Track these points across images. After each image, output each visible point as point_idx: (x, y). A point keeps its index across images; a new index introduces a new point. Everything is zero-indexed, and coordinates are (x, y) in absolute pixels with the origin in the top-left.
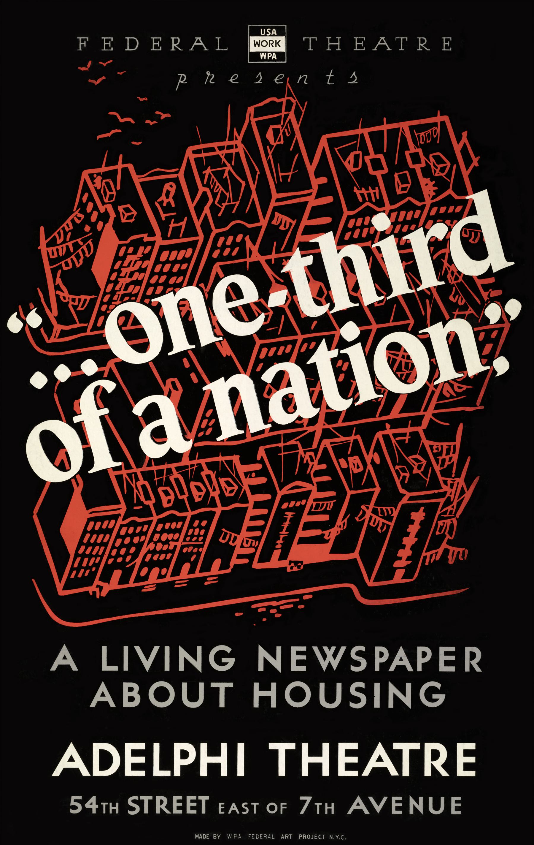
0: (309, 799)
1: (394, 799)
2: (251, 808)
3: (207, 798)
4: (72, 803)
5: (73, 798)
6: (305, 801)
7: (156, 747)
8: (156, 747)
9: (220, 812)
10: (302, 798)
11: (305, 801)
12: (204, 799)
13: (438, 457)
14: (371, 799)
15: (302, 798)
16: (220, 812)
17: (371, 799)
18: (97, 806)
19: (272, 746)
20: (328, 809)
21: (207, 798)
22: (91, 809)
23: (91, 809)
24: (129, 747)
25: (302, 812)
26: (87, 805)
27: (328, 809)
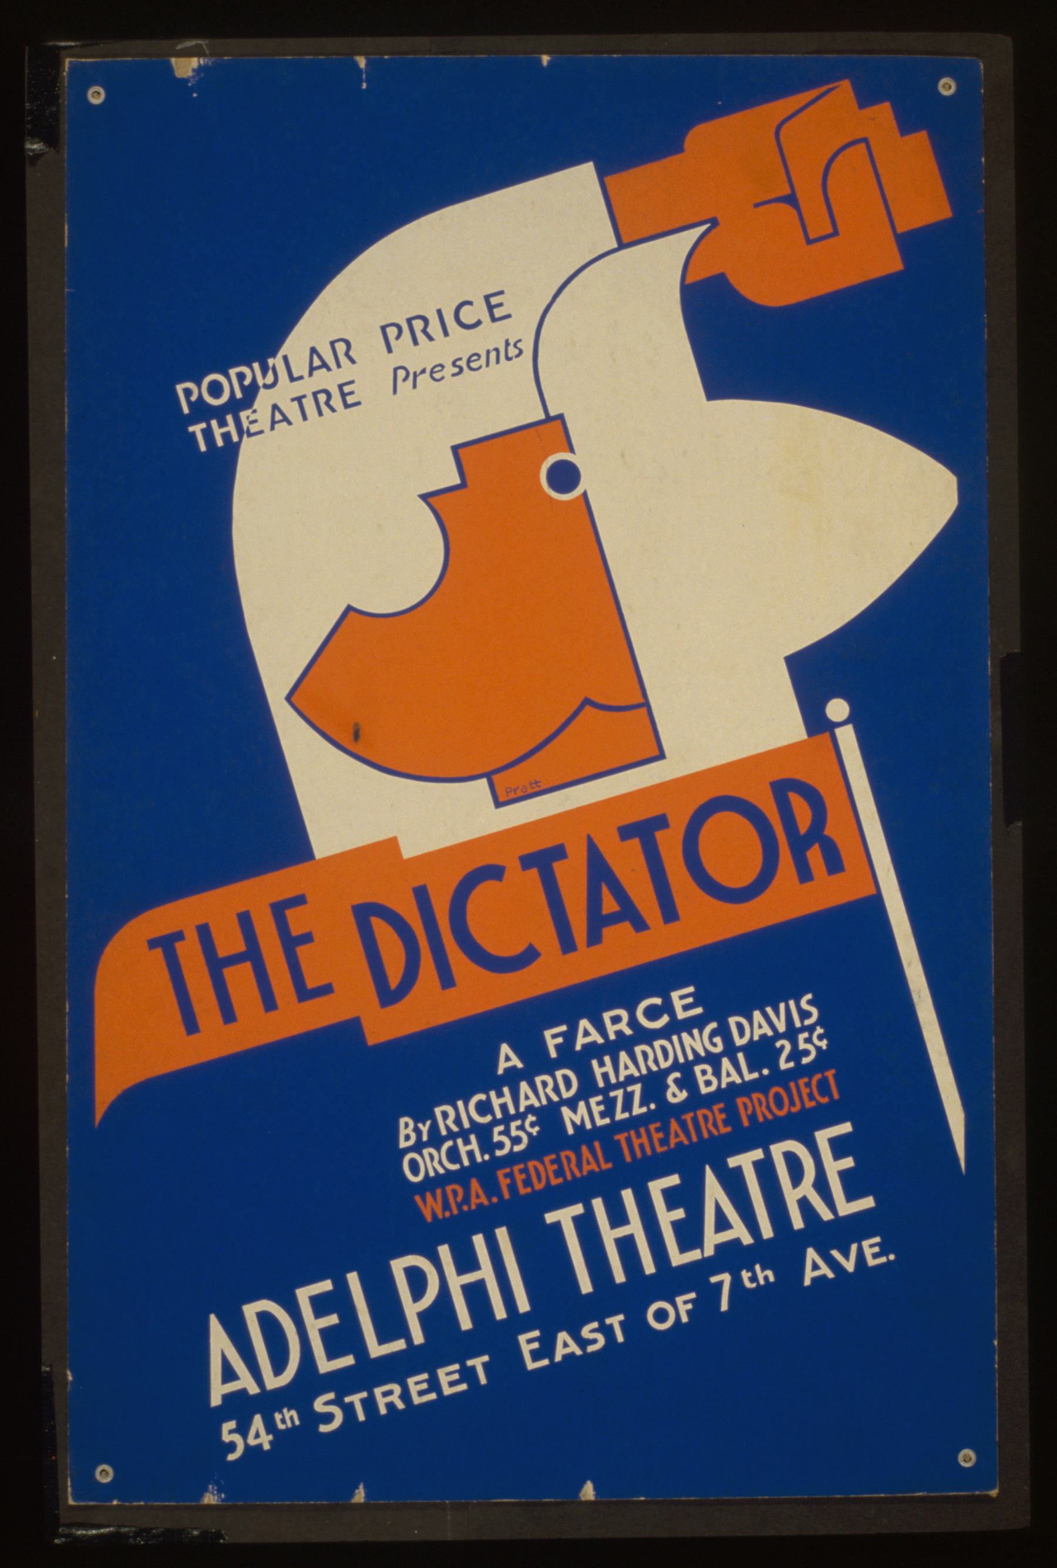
0: (726, 1278)
1: (865, 1244)
2: (607, 1331)
3: (621, 1317)
4: (226, 1438)
5: (294, 1413)
6: (720, 1284)
7: (353, 1279)
8: (353, 1279)
9: (531, 1365)
10: (714, 1279)
11: (720, 1284)
12: (615, 1321)
13: (683, 1117)
14: (835, 1253)
15: (714, 1279)
16: (531, 1365)
17: (835, 1253)
18: (270, 1437)
19: (550, 1218)
20: (467, 1289)
21: (621, 1317)
22: (260, 1446)
23: (260, 1446)
24: (304, 1295)
25: (724, 1306)
26: (252, 1441)
27: (467, 1289)
